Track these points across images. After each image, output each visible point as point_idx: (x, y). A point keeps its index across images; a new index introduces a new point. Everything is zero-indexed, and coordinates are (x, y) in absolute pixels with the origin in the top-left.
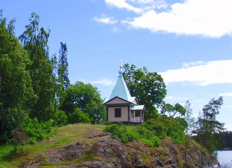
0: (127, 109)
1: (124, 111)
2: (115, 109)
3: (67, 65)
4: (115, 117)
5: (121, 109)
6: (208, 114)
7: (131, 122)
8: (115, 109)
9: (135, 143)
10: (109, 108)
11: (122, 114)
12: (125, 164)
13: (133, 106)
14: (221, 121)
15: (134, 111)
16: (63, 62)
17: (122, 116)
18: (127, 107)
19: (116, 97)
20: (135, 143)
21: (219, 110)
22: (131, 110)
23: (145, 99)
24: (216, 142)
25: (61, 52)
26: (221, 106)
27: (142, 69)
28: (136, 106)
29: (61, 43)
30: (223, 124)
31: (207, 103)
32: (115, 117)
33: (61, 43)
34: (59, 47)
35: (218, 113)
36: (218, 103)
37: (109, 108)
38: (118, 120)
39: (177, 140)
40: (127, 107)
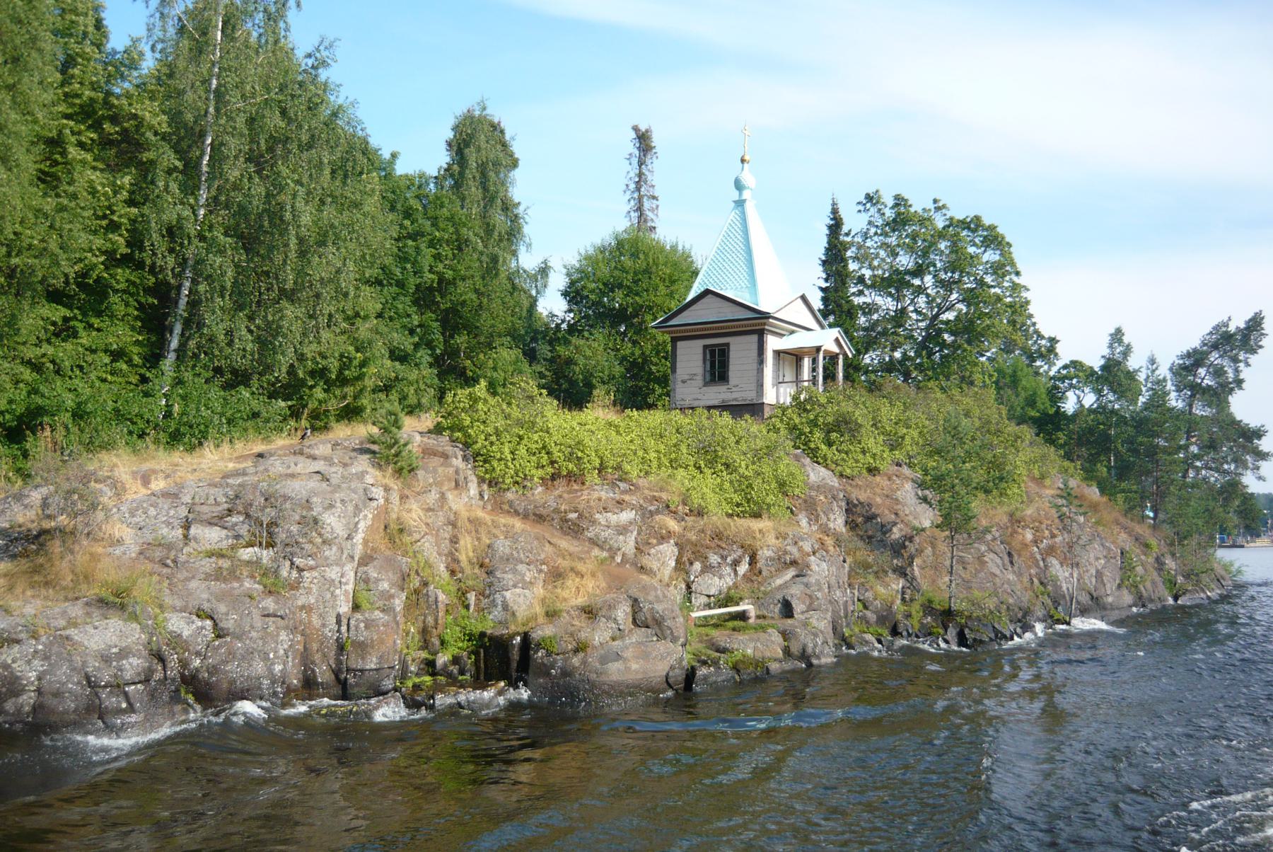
0: (755, 346)
2: (705, 347)
5: (728, 345)
6: (1196, 390)
8: (705, 347)
9: (920, 493)
10: (679, 344)
11: (731, 367)
12: (339, 622)
14: (1252, 421)
18: (755, 338)
19: (707, 292)
20: (920, 493)
21: (1245, 373)
23: (939, 332)
25: (635, 161)
26: (1253, 359)
29: (636, 129)
30: (1258, 434)
31: (1194, 342)
33: (636, 129)
34: (629, 145)
35: (1239, 383)
36: (1239, 340)
38: (717, 394)
40: (755, 338)
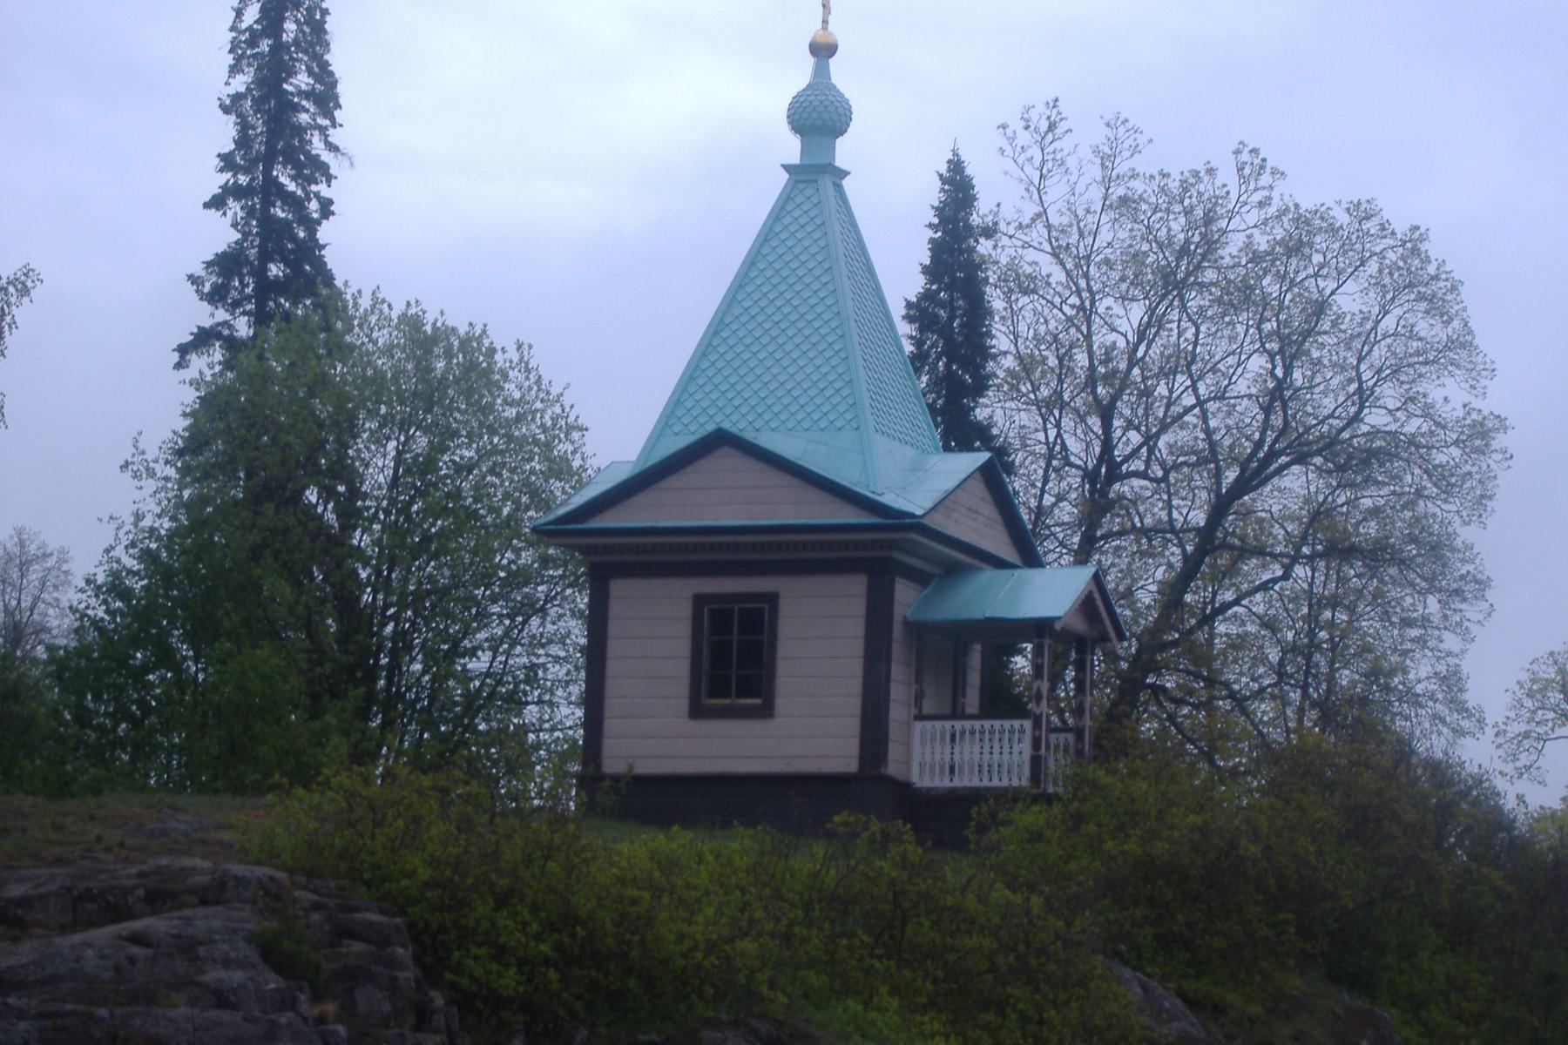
1: (818, 637)
2: (699, 601)
3: (326, 99)
4: (697, 711)
5: (772, 599)
7: (906, 786)
10: (618, 588)
13: (953, 572)
15: (961, 653)
16: (272, 74)
17: (782, 703)
18: (856, 586)
19: (718, 441)
22: (918, 631)
24: (553, 612)
27: (1227, 175)
28: (989, 574)
32: (697, 711)
37: (618, 588)
39: (503, 920)
40: (856, 586)
